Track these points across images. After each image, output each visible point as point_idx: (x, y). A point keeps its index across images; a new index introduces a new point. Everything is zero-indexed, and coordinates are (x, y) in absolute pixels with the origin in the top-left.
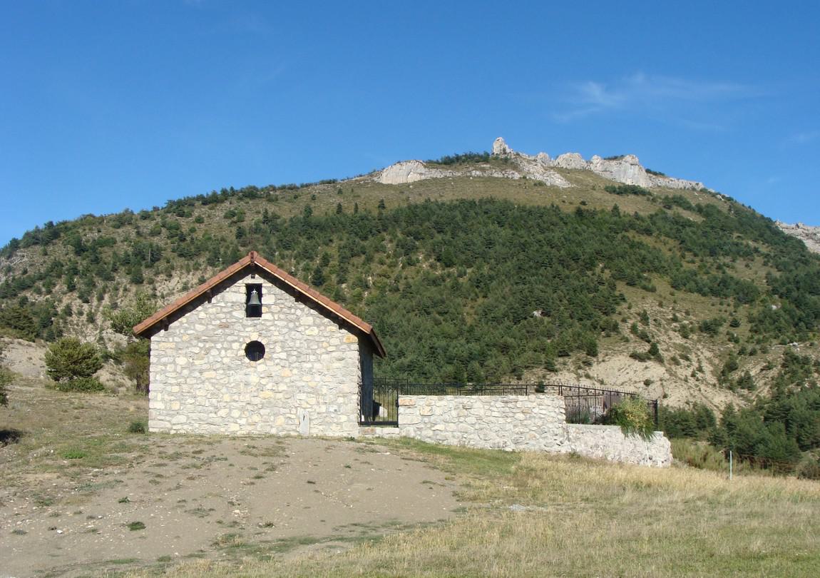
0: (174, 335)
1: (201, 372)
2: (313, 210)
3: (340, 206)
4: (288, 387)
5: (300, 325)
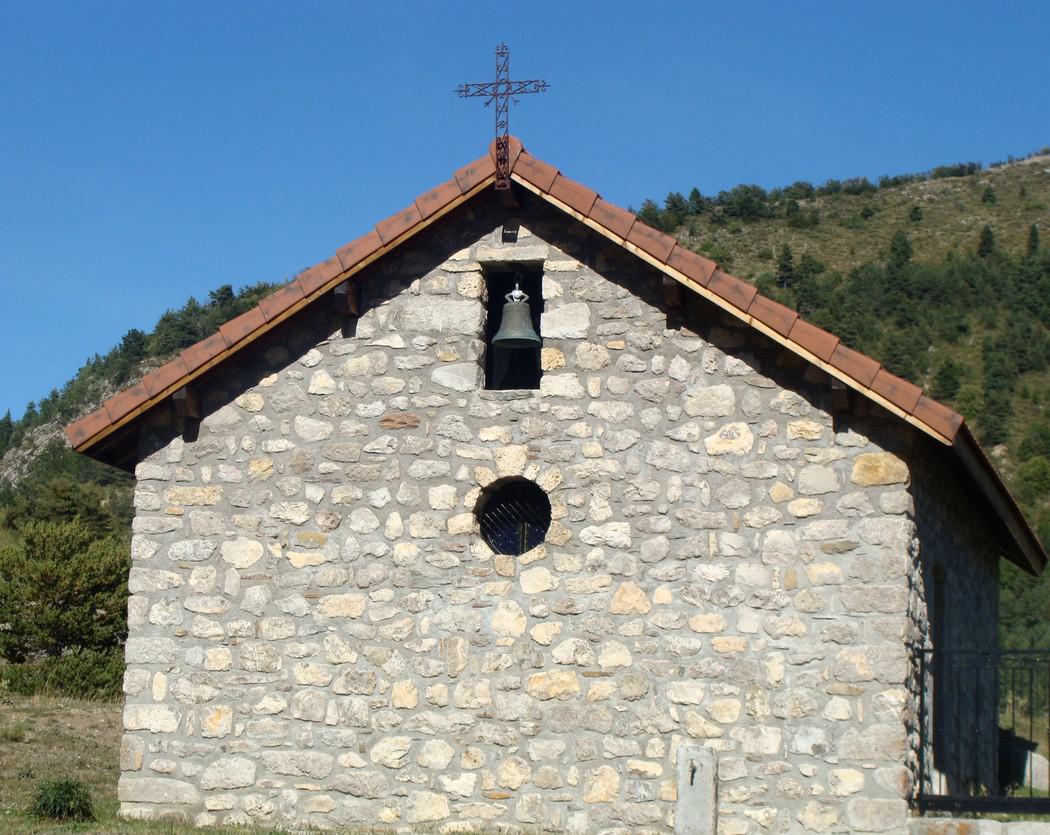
0: (217, 456)
1: (312, 595)
2: (914, 247)
3: (987, 237)
4: (637, 654)
5: (686, 417)
